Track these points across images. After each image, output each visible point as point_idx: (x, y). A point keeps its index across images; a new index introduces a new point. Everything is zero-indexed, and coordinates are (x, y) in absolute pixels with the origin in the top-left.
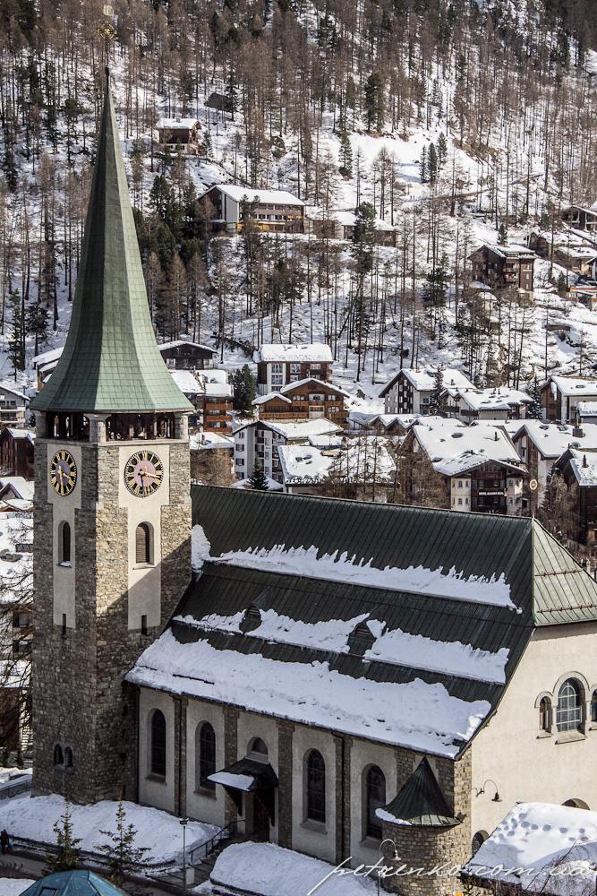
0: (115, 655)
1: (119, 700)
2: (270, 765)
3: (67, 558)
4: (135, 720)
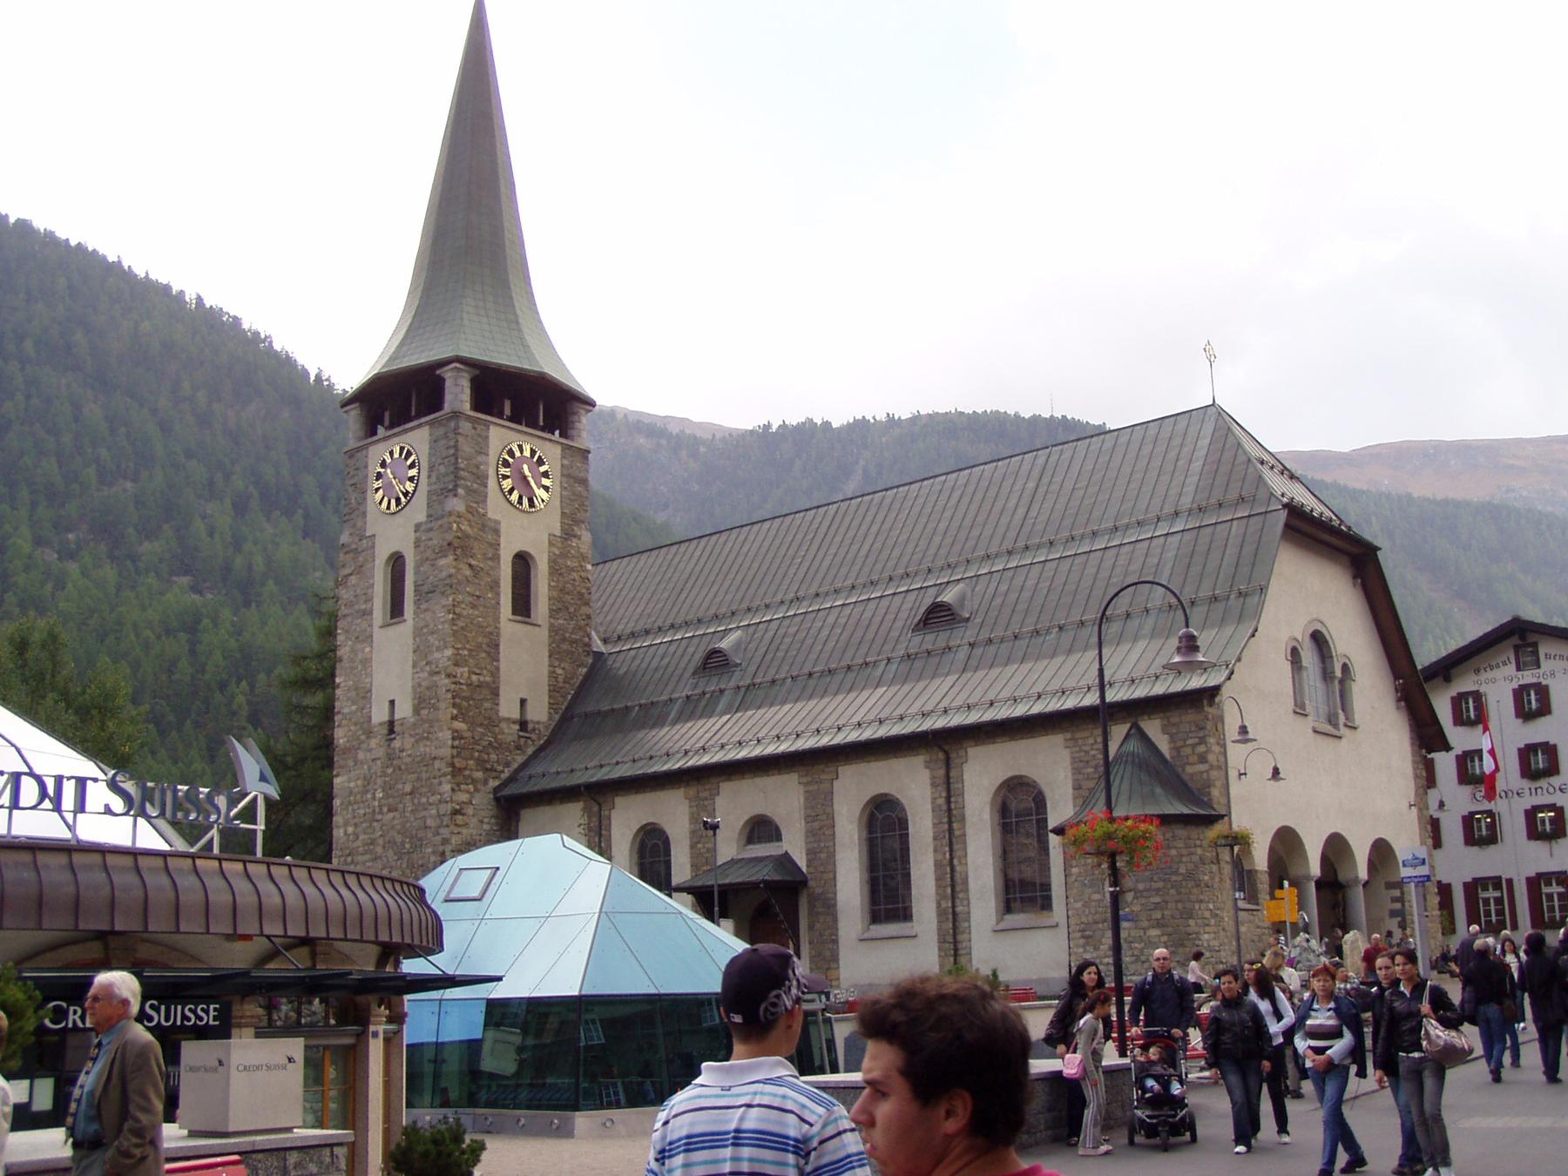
1: (486, 827)
3: (396, 609)
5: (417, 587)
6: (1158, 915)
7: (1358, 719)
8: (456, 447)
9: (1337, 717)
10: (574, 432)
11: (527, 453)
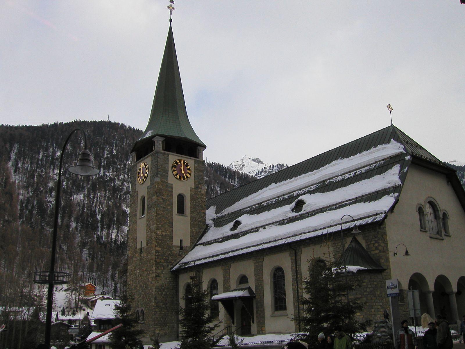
0: (166, 257)
1: (167, 280)
2: (250, 287)
3: (143, 214)
4: (176, 293)
5: (148, 205)
8: (157, 162)
10: (199, 156)
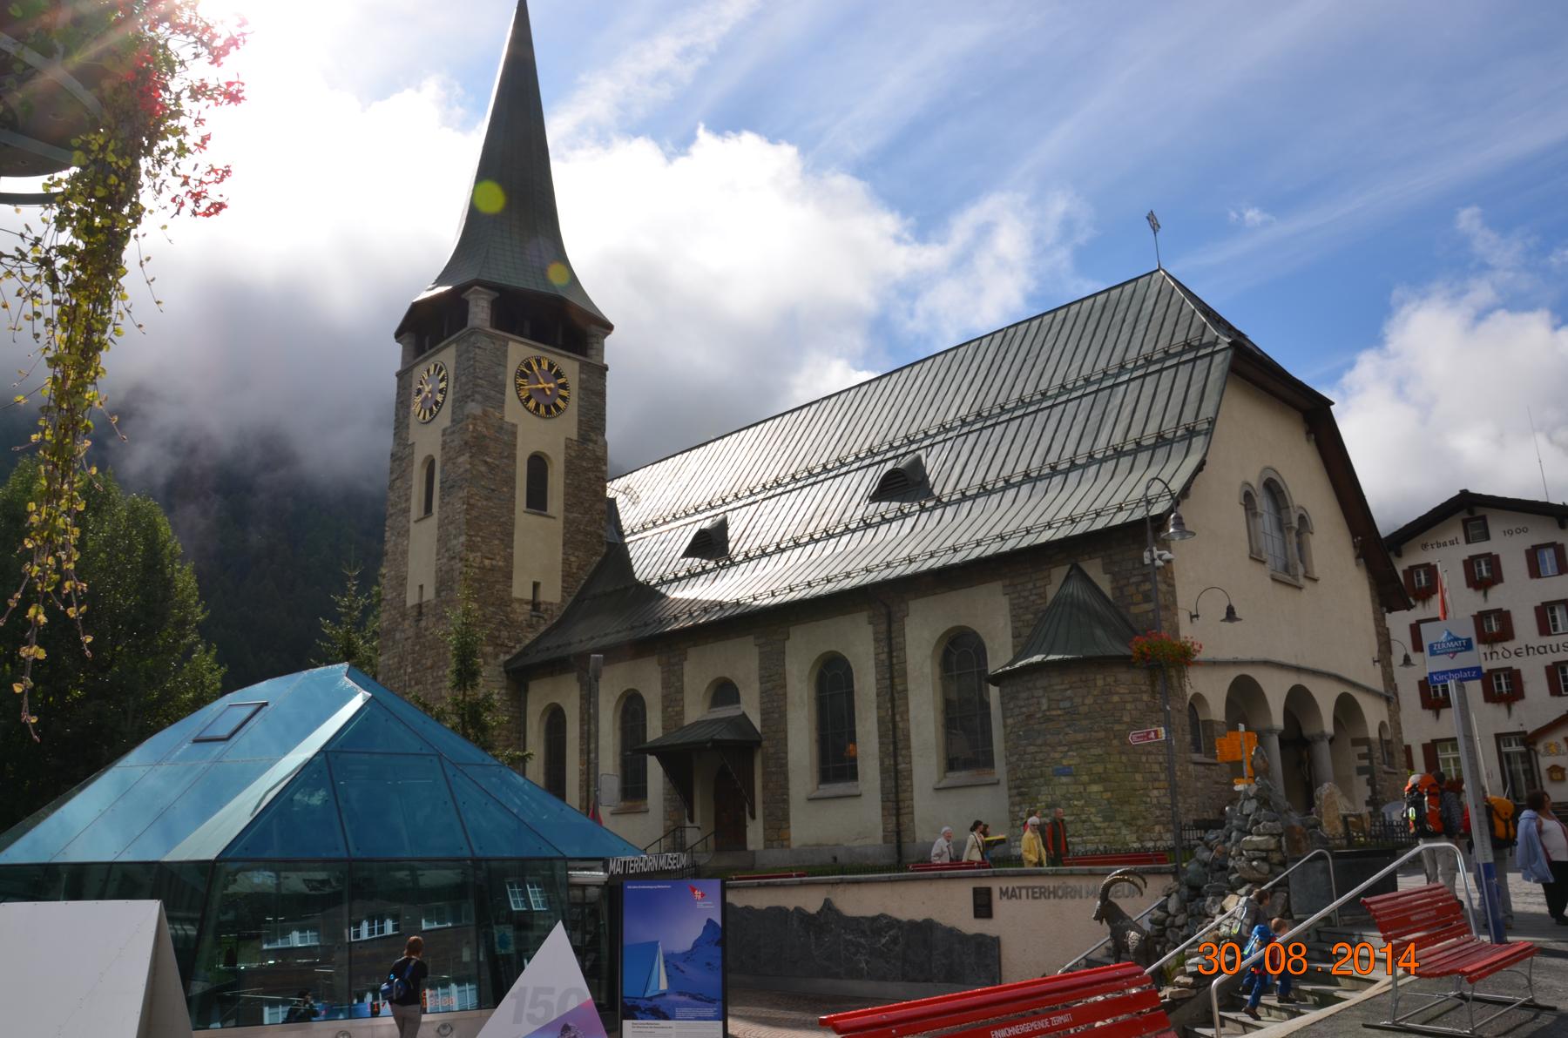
3: (428, 509)
6: (1099, 768)
7: (1317, 572)
9: (1293, 572)
10: (593, 352)
11: (545, 366)
